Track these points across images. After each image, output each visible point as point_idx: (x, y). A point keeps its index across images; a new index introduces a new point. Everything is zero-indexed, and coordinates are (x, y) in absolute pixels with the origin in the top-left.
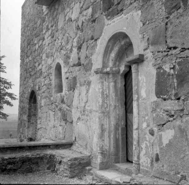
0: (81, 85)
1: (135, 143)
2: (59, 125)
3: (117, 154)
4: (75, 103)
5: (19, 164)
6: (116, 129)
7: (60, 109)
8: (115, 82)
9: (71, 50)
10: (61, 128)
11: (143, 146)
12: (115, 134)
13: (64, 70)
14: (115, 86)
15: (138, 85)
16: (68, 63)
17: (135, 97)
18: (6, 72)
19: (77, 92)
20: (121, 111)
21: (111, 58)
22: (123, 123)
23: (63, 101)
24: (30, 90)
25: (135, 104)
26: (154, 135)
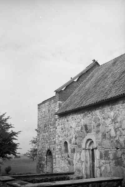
0: (77, 152)
1: (96, 171)
2: (67, 166)
3: (91, 175)
4: (75, 158)
5: (62, 154)
6: (90, 167)
7: (67, 160)
8: (89, 152)
9: (72, 138)
10: (68, 168)
11: (98, 171)
12: (90, 169)
13: (69, 145)
14: (89, 154)
15: (96, 155)
16: (71, 142)
17: (95, 158)
18: (5, 113)
19: (75, 154)
20: (91, 162)
21: (87, 145)
22: (92, 165)
23: (69, 157)
24: (46, 149)
25: (95, 160)
26: (7, 167)
